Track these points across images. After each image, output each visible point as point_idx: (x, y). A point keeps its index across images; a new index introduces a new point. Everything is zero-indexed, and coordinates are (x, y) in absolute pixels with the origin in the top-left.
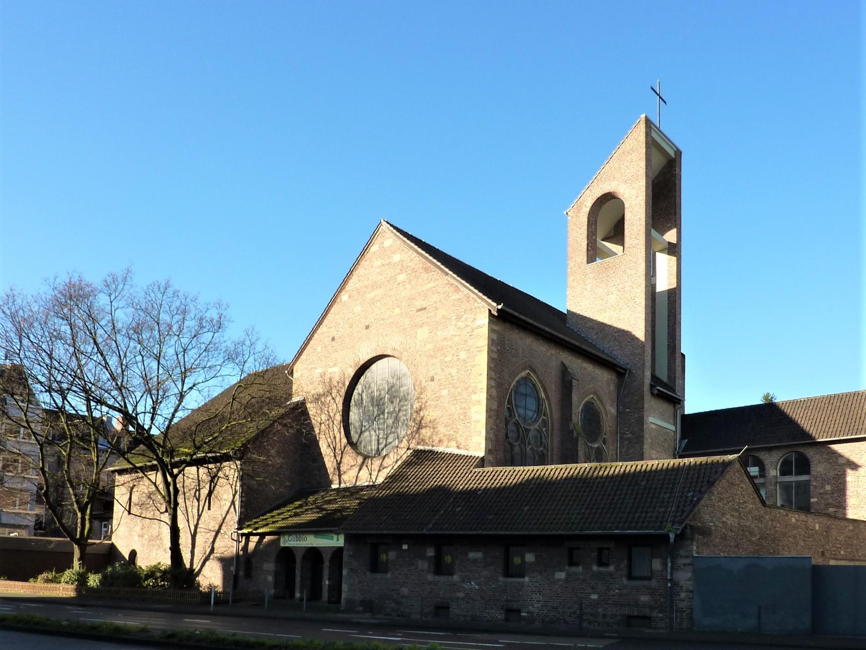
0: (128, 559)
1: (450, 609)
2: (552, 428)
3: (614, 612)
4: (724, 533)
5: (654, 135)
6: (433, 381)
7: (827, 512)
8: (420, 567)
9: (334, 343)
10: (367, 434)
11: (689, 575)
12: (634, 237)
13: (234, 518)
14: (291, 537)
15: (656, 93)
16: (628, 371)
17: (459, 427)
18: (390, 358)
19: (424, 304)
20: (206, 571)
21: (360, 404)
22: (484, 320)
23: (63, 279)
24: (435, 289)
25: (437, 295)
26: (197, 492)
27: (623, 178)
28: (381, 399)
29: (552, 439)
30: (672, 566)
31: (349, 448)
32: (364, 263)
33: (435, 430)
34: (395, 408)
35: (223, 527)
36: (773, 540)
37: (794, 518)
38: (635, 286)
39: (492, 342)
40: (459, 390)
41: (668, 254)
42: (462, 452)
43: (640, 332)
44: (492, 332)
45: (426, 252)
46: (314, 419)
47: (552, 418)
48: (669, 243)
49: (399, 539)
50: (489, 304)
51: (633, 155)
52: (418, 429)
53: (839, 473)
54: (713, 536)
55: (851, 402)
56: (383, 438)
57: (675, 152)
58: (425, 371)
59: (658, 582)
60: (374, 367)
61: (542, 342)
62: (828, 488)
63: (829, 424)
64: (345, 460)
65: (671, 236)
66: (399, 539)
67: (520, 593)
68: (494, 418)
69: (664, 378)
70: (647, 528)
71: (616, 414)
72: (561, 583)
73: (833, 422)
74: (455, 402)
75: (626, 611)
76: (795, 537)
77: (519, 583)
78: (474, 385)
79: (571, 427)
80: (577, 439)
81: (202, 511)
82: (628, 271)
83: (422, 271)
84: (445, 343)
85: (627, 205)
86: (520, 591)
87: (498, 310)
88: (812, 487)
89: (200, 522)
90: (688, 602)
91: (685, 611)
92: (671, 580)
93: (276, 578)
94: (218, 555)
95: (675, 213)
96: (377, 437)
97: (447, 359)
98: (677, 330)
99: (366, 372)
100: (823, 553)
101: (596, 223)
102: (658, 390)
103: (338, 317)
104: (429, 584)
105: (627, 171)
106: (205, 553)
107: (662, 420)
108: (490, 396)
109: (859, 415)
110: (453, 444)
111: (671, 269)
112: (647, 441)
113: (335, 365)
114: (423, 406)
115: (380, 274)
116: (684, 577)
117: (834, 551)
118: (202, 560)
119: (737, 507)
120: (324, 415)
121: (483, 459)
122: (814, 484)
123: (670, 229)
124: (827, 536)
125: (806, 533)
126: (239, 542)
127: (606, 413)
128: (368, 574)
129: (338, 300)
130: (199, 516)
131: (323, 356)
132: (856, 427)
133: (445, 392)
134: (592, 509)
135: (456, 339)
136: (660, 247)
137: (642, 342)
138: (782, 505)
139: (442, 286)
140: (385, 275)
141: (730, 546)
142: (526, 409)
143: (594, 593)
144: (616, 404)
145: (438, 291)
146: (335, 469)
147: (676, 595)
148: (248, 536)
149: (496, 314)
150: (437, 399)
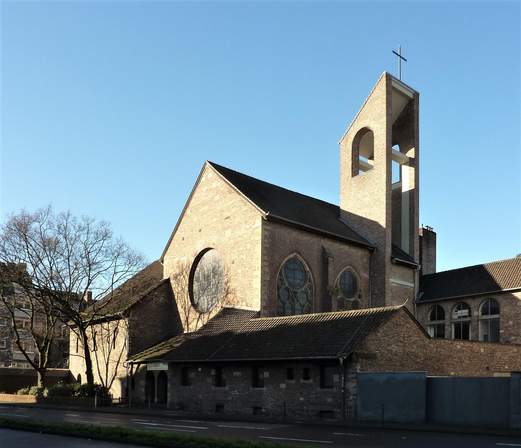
0: (77, 379)
1: (224, 407)
2: (315, 290)
3: (313, 408)
5: (394, 84)
9: (184, 242)
10: (202, 298)
11: (355, 384)
12: (379, 157)
13: (126, 352)
14: (152, 365)
15: (398, 55)
16: (376, 249)
17: (247, 293)
18: (213, 250)
19: (228, 214)
20: (113, 386)
21: (198, 280)
22: (259, 223)
23: (18, 213)
24: (234, 204)
25: (235, 208)
26: (108, 338)
27: (373, 117)
28: (209, 276)
29: (315, 297)
31: (192, 308)
33: (235, 295)
34: (216, 281)
35: (121, 359)
36: (438, 361)
37: (459, 345)
38: (380, 191)
39: (264, 238)
40: (247, 269)
41: (409, 166)
42: (249, 309)
43: (383, 222)
45: (229, 181)
46: (174, 290)
48: (410, 158)
49: (196, 365)
50: (262, 213)
51: (379, 100)
52: (227, 294)
53: (518, 312)
56: (210, 300)
57: (414, 94)
58: (229, 258)
60: (205, 256)
61: (306, 234)
63: (513, 278)
64: (190, 316)
65: (411, 153)
66: (196, 365)
67: (261, 397)
70: (328, 355)
73: (516, 277)
74: (245, 277)
77: (260, 391)
78: (254, 265)
79: (328, 289)
80: (331, 297)
81: (111, 351)
82: (376, 181)
84: (240, 239)
86: (261, 396)
87: (267, 217)
88: (500, 323)
89: (110, 357)
90: (354, 402)
91: (352, 408)
92: (344, 388)
94: (119, 376)
95: (414, 137)
96: (207, 300)
97: (241, 249)
98: (416, 218)
99: (201, 259)
100: (488, 368)
101: (358, 149)
102: (396, 260)
103: (185, 225)
105: (375, 112)
106: (112, 375)
107: (402, 280)
110: (244, 303)
111: (411, 176)
114: (229, 280)
115: (206, 196)
116: (352, 386)
118: (111, 380)
120: (179, 287)
121: (259, 312)
122: (502, 320)
127: (360, 277)
128: (181, 386)
129: (185, 214)
130: (110, 352)
133: (239, 271)
134: (304, 343)
136: (404, 162)
137: (384, 229)
139: (238, 202)
140: (209, 197)
142: (294, 278)
143: (302, 397)
145: (236, 205)
146: (185, 321)
147: (347, 397)
148: (132, 364)
150: (236, 275)
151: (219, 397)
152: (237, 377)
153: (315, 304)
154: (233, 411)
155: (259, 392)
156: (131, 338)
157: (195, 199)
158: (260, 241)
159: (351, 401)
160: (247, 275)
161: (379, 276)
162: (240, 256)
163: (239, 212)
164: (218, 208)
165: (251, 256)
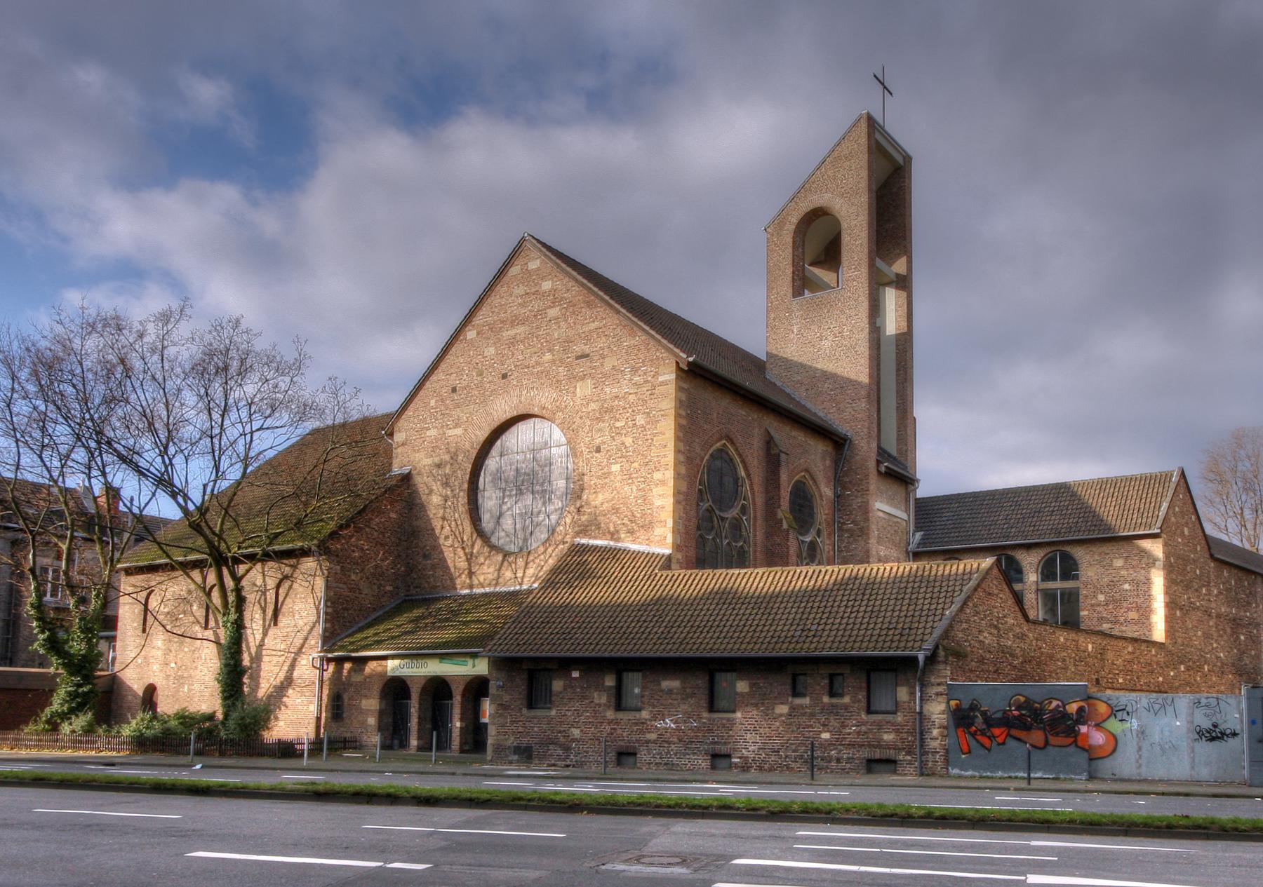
1: (638, 756)
4: (981, 656)
5: (878, 136)
6: (600, 451)
7: (1100, 628)
8: (596, 701)
16: (848, 442)
19: (587, 349)
22: (668, 376)
29: (755, 530)
30: (921, 697)
32: (501, 289)
37: (1062, 637)
40: (636, 465)
44: (680, 390)
47: (754, 504)
49: (565, 664)
50: (676, 355)
53: (1115, 579)
54: (969, 659)
55: (1127, 489)
59: (905, 716)
62: (1101, 598)
65: (899, 267)
67: (731, 732)
68: (683, 503)
69: (893, 451)
71: (833, 496)
72: (784, 718)
74: (630, 481)
75: (866, 753)
76: (1064, 660)
77: (728, 720)
83: (582, 305)
85: (844, 225)
87: (689, 364)
88: (1081, 597)
91: (938, 752)
93: (380, 721)
97: (618, 424)
100: (1097, 681)
101: (803, 245)
104: (609, 723)
107: (891, 505)
108: (679, 475)
109: (1137, 506)
112: (874, 533)
113: (457, 426)
117: (1111, 679)
119: (996, 623)
121: (669, 558)
123: (898, 256)
124: (1102, 660)
125: (1077, 655)
126: (323, 670)
131: (439, 413)
132: (1134, 521)
135: (632, 398)
138: (1045, 620)
141: (988, 671)
143: (825, 732)
144: (833, 483)
149: (686, 369)
151: (625, 734)
152: (670, 692)
153: (755, 545)
154: (661, 763)
155: (724, 721)
156: (332, 603)
157: (492, 308)
158: (673, 412)
159: (936, 739)
160: (637, 478)
161: (856, 497)
162: (616, 438)
163: (615, 349)
164: (556, 335)
165: (647, 440)
